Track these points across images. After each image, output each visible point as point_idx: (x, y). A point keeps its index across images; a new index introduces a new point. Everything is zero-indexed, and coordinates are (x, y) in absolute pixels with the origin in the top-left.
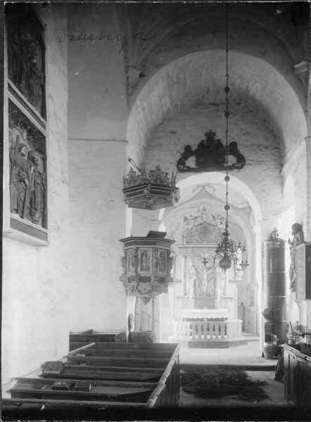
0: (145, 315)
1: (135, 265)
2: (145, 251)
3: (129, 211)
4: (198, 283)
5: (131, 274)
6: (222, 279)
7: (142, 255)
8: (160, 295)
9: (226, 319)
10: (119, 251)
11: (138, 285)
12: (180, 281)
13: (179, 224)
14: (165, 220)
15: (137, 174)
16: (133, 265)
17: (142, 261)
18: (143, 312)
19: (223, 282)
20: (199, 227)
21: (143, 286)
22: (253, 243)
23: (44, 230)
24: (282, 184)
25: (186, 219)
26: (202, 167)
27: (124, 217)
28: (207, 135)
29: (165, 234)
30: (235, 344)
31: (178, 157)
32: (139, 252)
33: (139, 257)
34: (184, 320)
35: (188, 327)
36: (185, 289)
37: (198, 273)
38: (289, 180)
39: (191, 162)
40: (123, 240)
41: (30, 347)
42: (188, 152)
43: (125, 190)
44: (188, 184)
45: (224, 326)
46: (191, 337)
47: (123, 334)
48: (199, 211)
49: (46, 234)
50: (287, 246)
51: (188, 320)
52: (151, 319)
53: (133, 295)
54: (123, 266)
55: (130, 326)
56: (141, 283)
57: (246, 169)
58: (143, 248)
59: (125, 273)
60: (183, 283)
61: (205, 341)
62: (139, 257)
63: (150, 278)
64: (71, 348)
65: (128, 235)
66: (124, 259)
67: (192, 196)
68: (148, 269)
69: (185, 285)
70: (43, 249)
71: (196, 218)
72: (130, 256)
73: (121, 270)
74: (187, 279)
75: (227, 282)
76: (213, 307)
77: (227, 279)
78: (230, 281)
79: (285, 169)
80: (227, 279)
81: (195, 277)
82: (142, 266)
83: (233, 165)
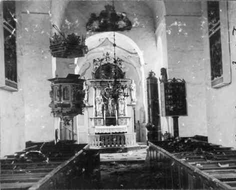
0: (67, 130)
1: (60, 96)
2: (66, 87)
3: (54, 60)
4: (105, 107)
5: (56, 102)
6: (123, 103)
7: (64, 89)
8: (77, 116)
9: (126, 132)
10: (48, 87)
11: (62, 109)
12: (92, 106)
13: (90, 64)
14: (80, 66)
15: (59, 37)
16: (58, 96)
17: (64, 93)
18: (66, 129)
19: (123, 106)
20: (105, 67)
21: (65, 110)
22: (141, 75)
23: (16, 83)
24: (156, 40)
25: (94, 61)
26: (103, 28)
27: (51, 63)
28: (106, 7)
29: (78, 76)
30: (132, 149)
31: (87, 21)
32: (62, 88)
33: (62, 91)
34: (89, 129)
35: (99, 139)
36: (96, 112)
37: (105, 100)
38: (159, 39)
39: (96, 25)
40: (50, 80)
41: (5, 143)
42: (94, 18)
43: (51, 47)
44: (93, 41)
45: (123, 137)
46: (100, 147)
47: (53, 142)
48: (104, 55)
49: (17, 85)
50: (159, 82)
51: (98, 134)
52: (71, 134)
53: (59, 117)
54: (51, 97)
55: (57, 137)
56: (64, 108)
57: (131, 32)
58: (64, 85)
59: (53, 102)
60: (94, 107)
61: (111, 148)
62: (62, 91)
63: (69, 105)
64: (26, 147)
65: (54, 77)
66: (52, 93)
67: (99, 44)
68: (68, 99)
69: (96, 108)
70: (14, 93)
71: (102, 60)
72: (56, 91)
73: (50, 100)
74: (97, 105)
75: (232, 63)
76: (114, 124)
77: (126, 104)
78: (128, 105)
79: (156, 32)
80: (126, 104)
81: (103, 103)
82: (64, 97)
83: (125, 27)
